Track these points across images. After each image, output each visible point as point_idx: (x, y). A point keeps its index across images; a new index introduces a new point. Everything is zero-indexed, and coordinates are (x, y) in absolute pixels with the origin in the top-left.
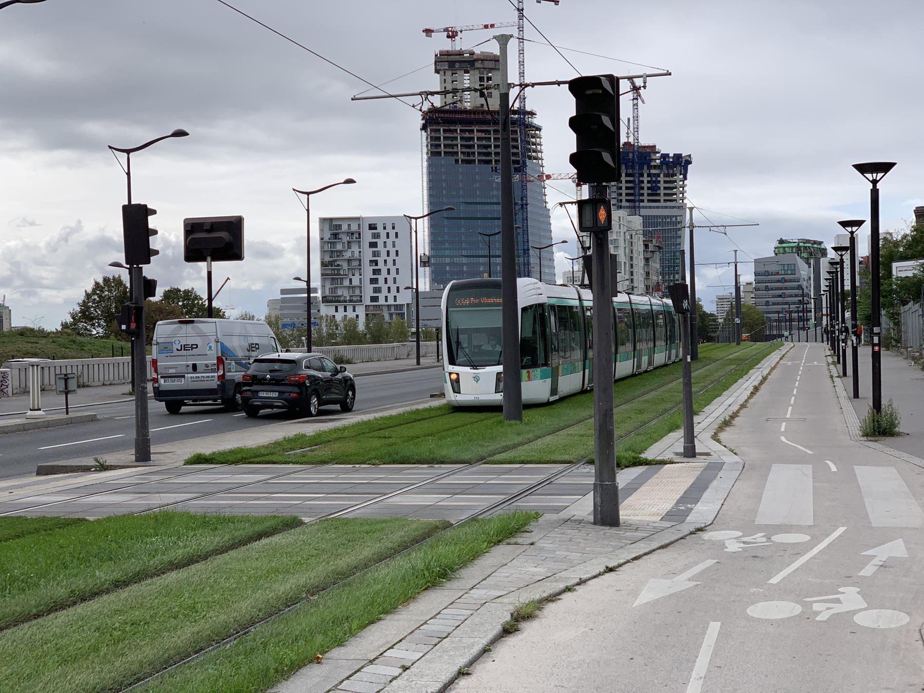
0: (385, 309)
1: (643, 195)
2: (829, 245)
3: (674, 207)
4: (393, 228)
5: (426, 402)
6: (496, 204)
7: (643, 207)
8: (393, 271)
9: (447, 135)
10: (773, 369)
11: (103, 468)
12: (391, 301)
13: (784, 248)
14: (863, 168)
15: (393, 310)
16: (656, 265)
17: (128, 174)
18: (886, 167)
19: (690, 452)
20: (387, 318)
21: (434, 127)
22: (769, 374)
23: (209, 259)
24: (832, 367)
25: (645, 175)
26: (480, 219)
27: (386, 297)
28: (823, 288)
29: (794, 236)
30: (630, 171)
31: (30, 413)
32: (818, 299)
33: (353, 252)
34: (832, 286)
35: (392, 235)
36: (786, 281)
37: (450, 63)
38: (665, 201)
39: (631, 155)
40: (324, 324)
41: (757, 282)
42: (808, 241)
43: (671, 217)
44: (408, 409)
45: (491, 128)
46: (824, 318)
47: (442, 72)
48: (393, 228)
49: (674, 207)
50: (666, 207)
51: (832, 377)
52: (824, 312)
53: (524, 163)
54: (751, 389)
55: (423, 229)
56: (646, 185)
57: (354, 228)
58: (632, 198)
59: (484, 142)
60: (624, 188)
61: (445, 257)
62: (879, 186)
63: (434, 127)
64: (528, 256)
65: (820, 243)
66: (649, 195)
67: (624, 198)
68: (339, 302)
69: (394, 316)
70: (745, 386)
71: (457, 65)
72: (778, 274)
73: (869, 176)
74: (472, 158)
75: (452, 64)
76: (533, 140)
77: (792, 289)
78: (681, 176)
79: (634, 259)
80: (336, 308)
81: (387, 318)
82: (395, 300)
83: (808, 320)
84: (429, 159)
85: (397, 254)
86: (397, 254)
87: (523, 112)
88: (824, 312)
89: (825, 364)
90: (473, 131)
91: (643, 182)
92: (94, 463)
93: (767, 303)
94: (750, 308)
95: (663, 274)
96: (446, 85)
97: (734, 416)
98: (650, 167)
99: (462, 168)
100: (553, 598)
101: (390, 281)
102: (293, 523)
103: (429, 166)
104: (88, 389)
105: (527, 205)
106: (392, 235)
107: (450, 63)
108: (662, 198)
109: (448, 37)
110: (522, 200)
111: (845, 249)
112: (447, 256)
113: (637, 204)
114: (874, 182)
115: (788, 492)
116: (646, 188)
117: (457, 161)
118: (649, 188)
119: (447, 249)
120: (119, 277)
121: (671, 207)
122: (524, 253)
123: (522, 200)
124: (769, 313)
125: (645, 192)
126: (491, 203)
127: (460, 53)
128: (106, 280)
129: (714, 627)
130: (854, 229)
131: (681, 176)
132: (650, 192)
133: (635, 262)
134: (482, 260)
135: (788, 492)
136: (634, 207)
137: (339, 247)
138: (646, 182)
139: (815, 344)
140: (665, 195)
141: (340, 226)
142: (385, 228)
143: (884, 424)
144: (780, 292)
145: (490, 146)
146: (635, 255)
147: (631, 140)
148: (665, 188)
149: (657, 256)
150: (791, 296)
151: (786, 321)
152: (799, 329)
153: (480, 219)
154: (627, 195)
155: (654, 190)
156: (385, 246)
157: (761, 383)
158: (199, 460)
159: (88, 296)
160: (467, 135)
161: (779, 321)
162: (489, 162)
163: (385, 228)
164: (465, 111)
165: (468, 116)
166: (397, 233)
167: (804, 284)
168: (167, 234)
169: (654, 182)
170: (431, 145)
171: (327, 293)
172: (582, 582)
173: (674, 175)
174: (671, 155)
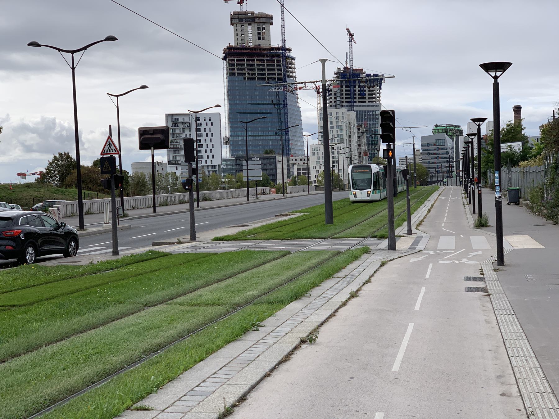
0: (206, 168)
1: (355, 98)
2: (466, 131)
3: (374, 106)
4: (210, 120)
5: (273, 219)
6: (269, 104)
7: (356, 106)
8: (210, 146)
9: (239, 63)
10: (436, 201)
11: (180, 243)
12: (209, 164)
13: (438, 130)
14: (487, 67)
15: (210, 169)
16: (364, 140)
17: (118, 107)
18: (503, 66)
19: (410, 232)
20: (207, 173)
21: (231, 58)
22: (434, 203)
23: (152, 148)
24: (464, 199)
25: (357, 87)
26: (259, 113)
27: (206, 161)
28: (460, 151)
29: (444, 123)
30: (348, 84)
31: (104, 225)
32: (458, 162)
33: (186, 135)
34: (466, 150)
35: (209, 124)
36: (439, 149)
37: (240, 19)
38: (369, 102)
39: (348, 75)
40: (170, 178)
41: (423, 150)
42: (452, 126)
43: (372, 111)
44: (264, 224)
45: (265, 59)
46: (461, 172)
47: (235, 25)
48: (210, 120)
49: (374, 106)
50: (369, 106)
51: (464, 204)
52: (461, 169)
53: (285, 79)
54: (427, 210)
55: (225, 120)
56: (357, 93)
57: (186, 120)
58: (349, 100)
59: (261, 67)
60: (344, 94)
61: (238, 136)
62: (499, 80)
63: (231, 58)
64: (288, 135)
65: (459, 127)
66: (359, 98)
67: (344, 100)
68: (178, 164)
69: (211, 173)
70: (424, 209)
71: (244, 20)
72: (435, 145)
73: (493, 74)
74: (254, 77)
75: (241, 20)
76: (290, 66)
77: (443, 154)
78: (378, 87)
79: (352, 137)
80: (177, 168)
81: (207, 173)
82: (212, 163)
83: (452, 172)
84: (228, 78)
85: (212, 136)
86: (212, 136)
87: (283, 49)
88: (461, 169)
89: (461, 198)
90: (254, 60)
91: (355, 91)
92: (177, 241)
93: (429, 163)
94: (419, 165)
95: (368, 145)
96: (238, 32)
97: (422, 221)
98: (359, 82)
99: (248, 83)
100: (389, 261)
101: (209, 151)
102: (289, 253)
103: (229, 82)
104: (92, 216)
105: (287, 104)
106: (209, 124)
107: (240, 19)
108: (367, 100)
109: (238, 3)
110: (284, 102)
111: (474, 135)
112: (240, 136)
113: (352, 104)
114: (496, 78)
115: (447, 242)
116: (357, 94)
117: (245, 79)
118: (359, 94)
119: (240, 131)
120: (68, 153)
121: (372, 106)
122: (286, 134)
123: (284, 102)
124: (430, 168)
125: (357, 96)
126: (265, 104)
127: (246, 13)
128: (60, 155)
129: (431, 265)
130: (473, 137)
131: (378, 87)
132: (360, 96)
133: (352, 139)
134: (270, 138)
135: (447, 242)
136: (351, 106)
137: (178, 131)
138: (357, 91)
139: (456, 187)
140: (369, 98)
141: (178, 119)
142: (205, 120)
143: (483, 222)
144: (436, 156)
145: (265, 70)
146: (352, 135)
147: (348, 66)
148: (369, 94)
149: (365, 135)
150: (442, 158)
151: (440, 172)
152: (447, 177)
153: (259, 113)
154: (346, 98)
155: (362, 95)
156: (205, 131)
157: (431, 207)
158: (217, 239)
159: (50, 164)
160: (251, 63)
161: (436, 173)
162: (264, 79)
163: (205, 120)
164: (249, 49)
165: (251, 51)
166: (212, 123)
167: (450, 151)
168: (62, 122)
169: (362, 91)
170: (229, 69)
171: (171, 159)
172: (394, 259)
173: (374, 86)
174: (372, 75)
